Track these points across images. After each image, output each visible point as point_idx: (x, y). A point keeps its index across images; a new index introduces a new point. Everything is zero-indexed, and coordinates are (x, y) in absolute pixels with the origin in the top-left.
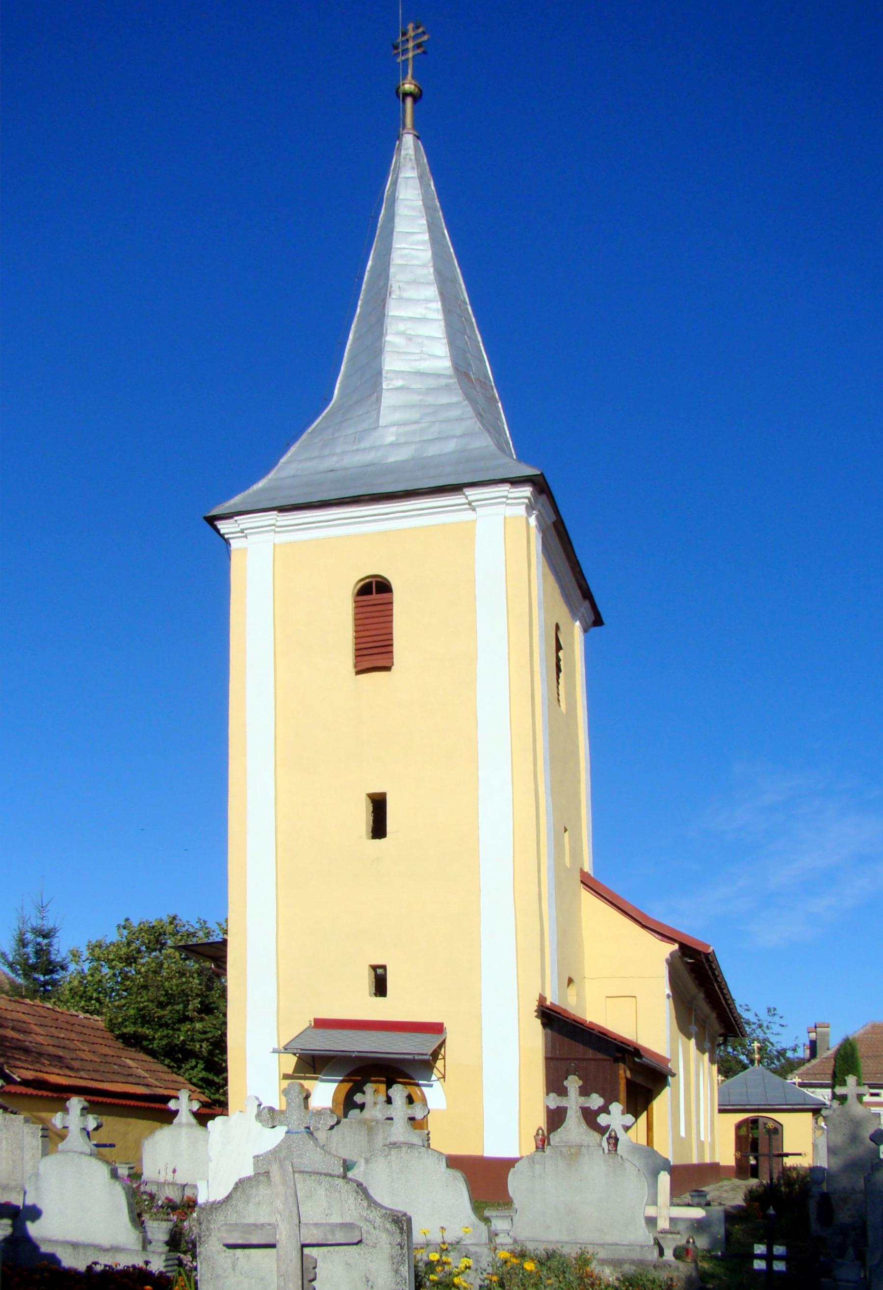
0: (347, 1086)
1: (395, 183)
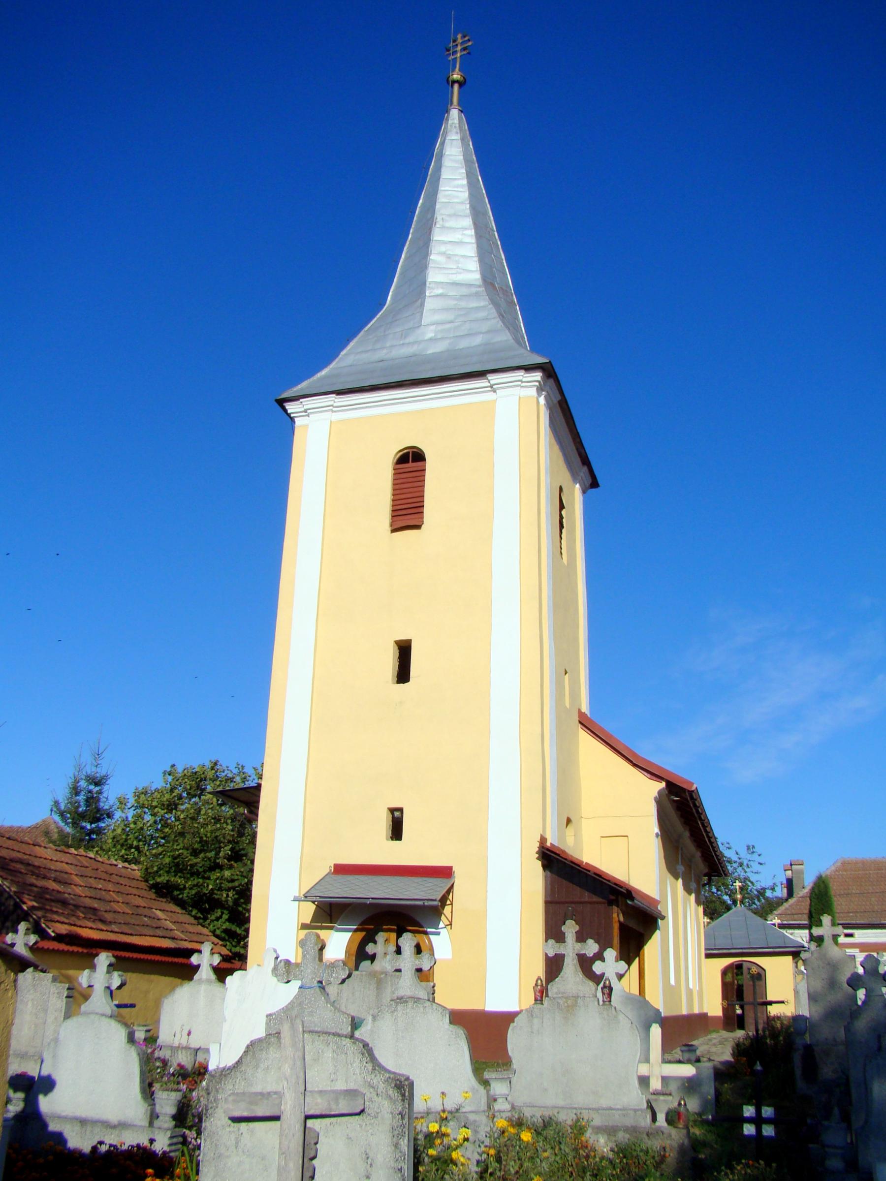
0: (361, 935)
1: (443, 143)
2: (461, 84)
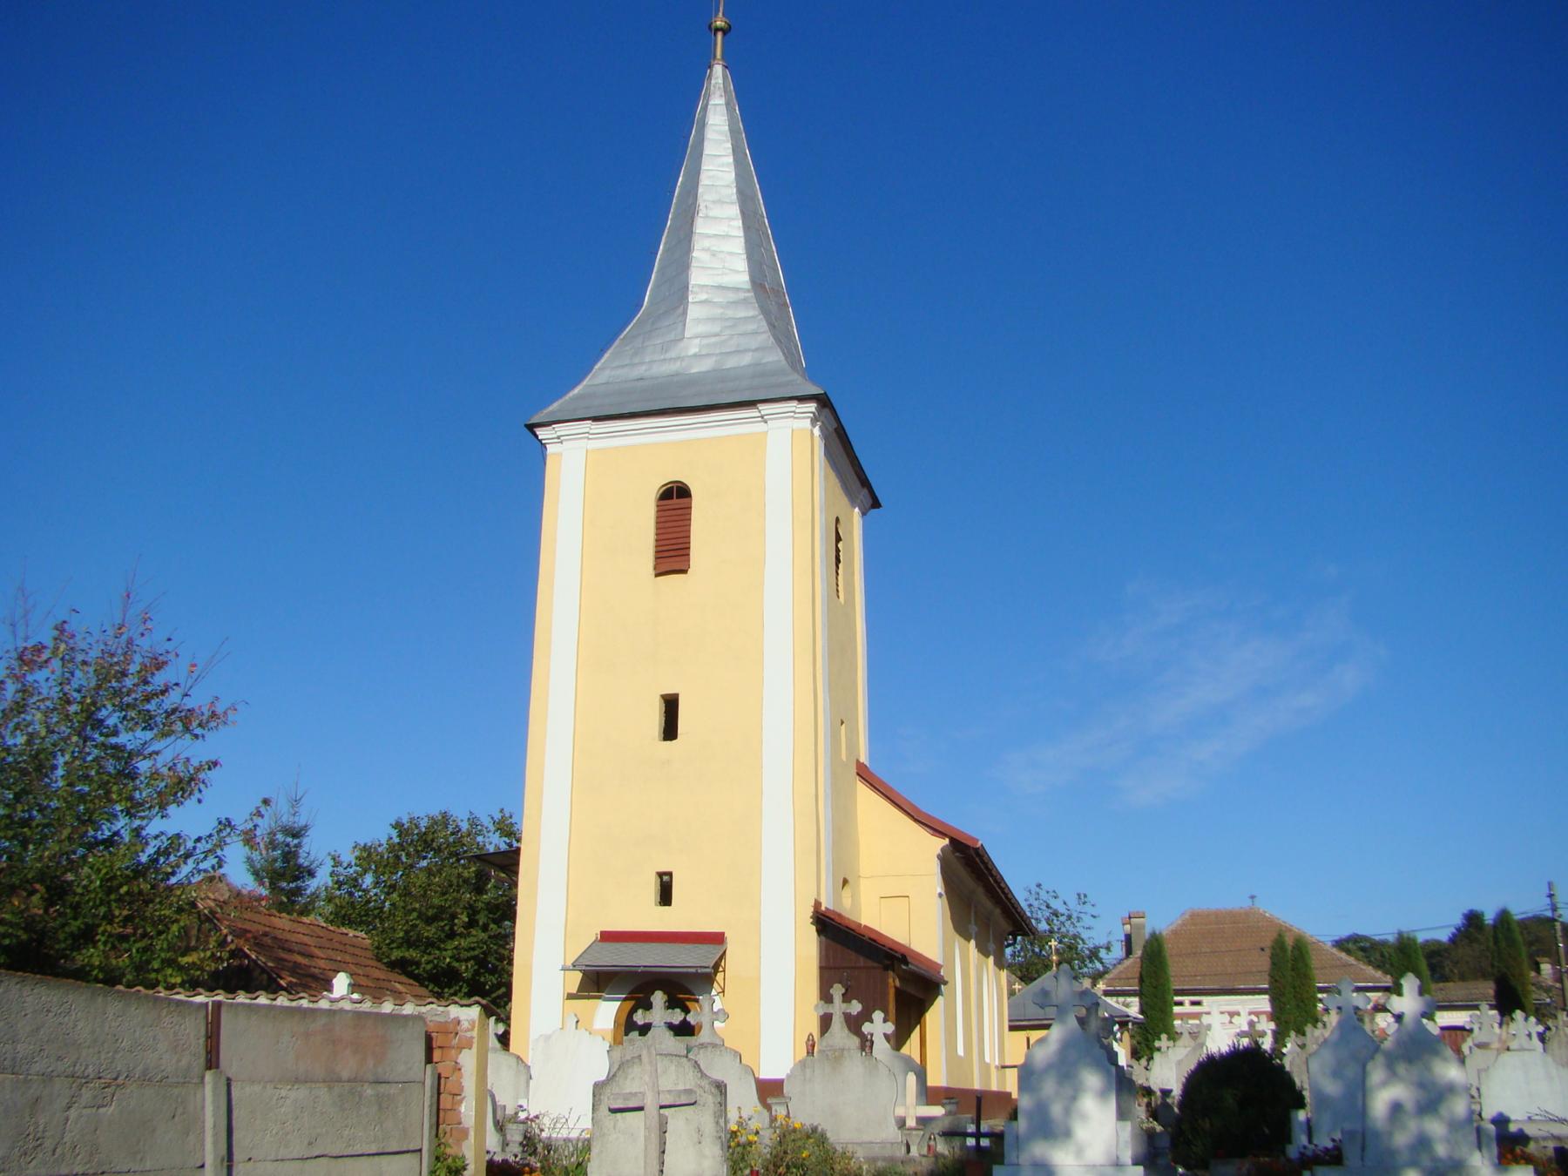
0: (630, 1004)
1: (705, 108)
2: (725, 32)
